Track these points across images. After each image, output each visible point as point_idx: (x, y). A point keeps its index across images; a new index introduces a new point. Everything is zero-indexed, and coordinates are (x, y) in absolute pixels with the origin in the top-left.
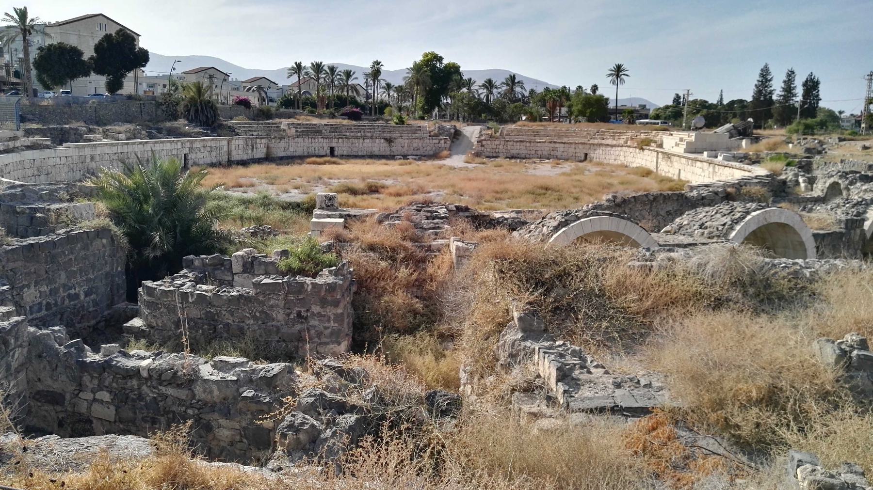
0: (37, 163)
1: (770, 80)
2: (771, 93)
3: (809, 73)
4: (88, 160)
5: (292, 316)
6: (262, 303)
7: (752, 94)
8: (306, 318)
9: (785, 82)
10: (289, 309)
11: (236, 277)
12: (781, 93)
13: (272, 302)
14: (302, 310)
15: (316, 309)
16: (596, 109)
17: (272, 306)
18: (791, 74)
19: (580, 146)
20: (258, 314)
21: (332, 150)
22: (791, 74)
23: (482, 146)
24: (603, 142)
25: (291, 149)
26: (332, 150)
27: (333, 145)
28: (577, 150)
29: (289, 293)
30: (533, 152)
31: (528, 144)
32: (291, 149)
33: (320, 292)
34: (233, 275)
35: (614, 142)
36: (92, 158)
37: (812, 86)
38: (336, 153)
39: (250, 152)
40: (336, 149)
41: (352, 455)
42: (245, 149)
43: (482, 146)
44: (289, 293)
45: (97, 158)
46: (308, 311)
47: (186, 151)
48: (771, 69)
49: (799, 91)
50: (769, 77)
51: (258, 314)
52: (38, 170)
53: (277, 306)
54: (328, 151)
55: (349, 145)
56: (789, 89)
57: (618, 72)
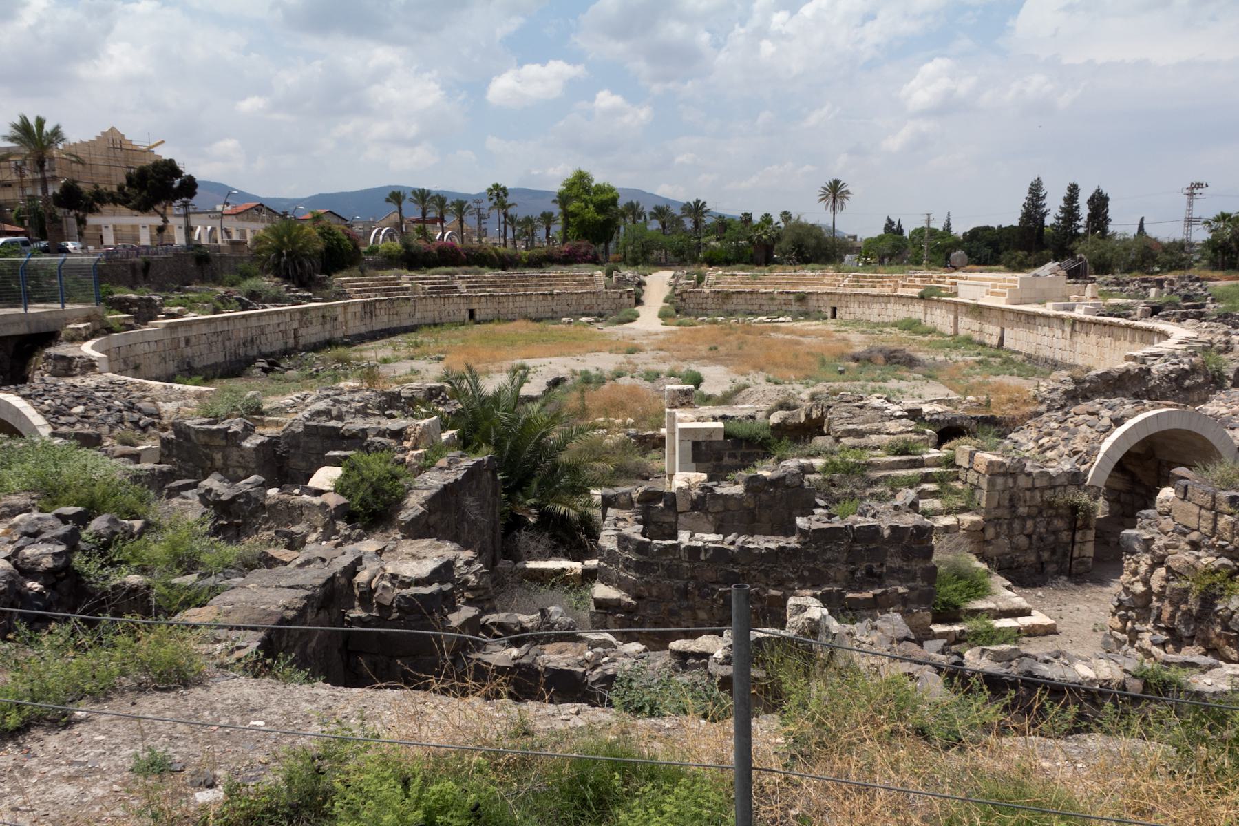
0: (123, 352)
1: (1044, 197)
2: (1044, 214)
3: (1032, 179)
4: (183, 344)
5: (859, 575)
6: (813, 557)
7: (1020, 216)
8: (880, 576)
9: (1065, 199)
10: (853, 564)
11: (681, 518)
12: (1059, 215)
13: (828, 556)
14: (874, 565)
15: (896, 562)
16: (815, 248)
17: (828, 561)
18: (1073, 190)
19: (825, 298)
20: (806, 573)
21: (472, 313)
22: (1073, 190)
23: (683, 300)
24: (860, 290)
25: (418, 315)
26: (472, 313)
27: (474, 306)
28: (821, 303)
29: (855, 540)
30: (756, 307)
31: (748, 296)
32: (418, 315)
33: (902, 539)
34: (677, 514)
35: (875, 291)
36: (187, 341)
37: (1099, 202)
38: (477, 317)
39: (368, 321)
40: (477, 312)
41: (66, 691)
42: (362, 319)
43: (683, 300)
44: (855, 540)
45: (193, 340)
46: (882, 565)
47: (296, 325)
48: (1043, 180)
49: (1084, 211)
50: (1042, 193)
51: (806, 573)
52: (125, 362)
53: (836, 560)
54: (467, 315)
55: (495, 305)
56: (1070, 211)
57: (835, 192)
